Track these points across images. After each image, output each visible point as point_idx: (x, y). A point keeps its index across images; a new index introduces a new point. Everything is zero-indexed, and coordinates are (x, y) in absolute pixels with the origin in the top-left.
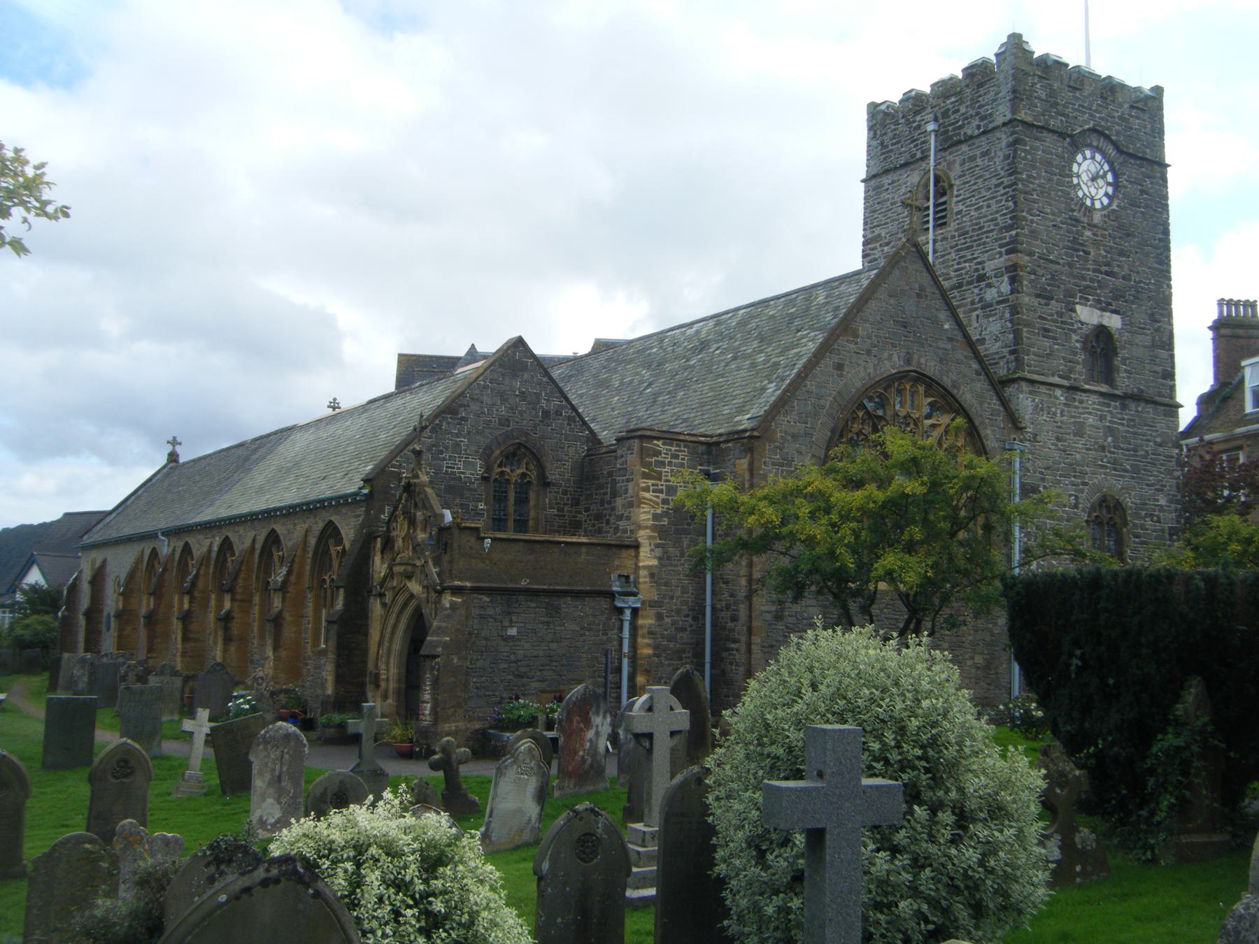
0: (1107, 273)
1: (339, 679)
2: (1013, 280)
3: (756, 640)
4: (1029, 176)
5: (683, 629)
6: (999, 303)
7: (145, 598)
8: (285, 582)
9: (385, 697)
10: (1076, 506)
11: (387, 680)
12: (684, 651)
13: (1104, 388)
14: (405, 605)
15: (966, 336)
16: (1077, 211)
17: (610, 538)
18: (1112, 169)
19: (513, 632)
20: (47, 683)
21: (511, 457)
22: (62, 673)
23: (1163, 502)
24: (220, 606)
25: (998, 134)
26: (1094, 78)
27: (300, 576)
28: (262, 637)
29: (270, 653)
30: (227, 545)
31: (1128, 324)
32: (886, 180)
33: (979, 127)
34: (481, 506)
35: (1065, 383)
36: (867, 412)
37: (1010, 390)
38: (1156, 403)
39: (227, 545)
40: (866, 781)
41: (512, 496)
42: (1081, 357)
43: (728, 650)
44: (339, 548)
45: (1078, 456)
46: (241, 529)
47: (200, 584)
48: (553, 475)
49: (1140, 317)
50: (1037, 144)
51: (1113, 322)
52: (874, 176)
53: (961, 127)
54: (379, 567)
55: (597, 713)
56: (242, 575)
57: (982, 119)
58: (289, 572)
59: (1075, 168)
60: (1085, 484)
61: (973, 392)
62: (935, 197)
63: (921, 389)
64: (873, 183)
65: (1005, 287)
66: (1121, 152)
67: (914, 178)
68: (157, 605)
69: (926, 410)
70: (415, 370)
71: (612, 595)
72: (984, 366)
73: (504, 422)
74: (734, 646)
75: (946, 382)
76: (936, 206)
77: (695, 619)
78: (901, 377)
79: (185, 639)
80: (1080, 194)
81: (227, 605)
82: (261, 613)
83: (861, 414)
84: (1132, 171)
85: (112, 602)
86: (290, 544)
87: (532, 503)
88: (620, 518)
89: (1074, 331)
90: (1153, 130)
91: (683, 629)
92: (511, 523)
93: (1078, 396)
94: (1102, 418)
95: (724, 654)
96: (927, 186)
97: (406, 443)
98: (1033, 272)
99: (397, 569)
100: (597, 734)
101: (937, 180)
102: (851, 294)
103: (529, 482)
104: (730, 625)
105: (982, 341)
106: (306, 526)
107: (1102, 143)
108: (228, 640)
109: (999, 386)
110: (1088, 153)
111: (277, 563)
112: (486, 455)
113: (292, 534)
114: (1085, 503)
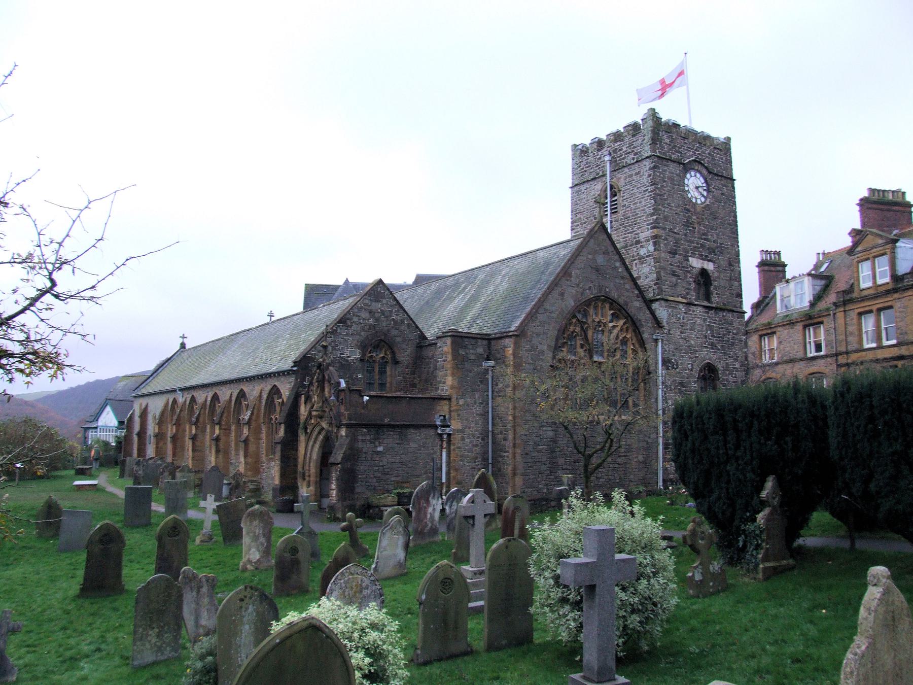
0: (705, 239)
1: (283, 475)
2: (655, 244)
3: (518, 451)
4: (662, 186)
5: (477, 445)
6: (648, 256)
7: (170, 426)
8: (250, 419)
9: (309, 486)
10: (692, 370)
11: (309, 476)
12: (477, 458)
13: (706, 303)
14: (319, 433)
15: (631, 275)
16: (688, 206)
17: (434, 394)
18: (706, 181)
19: (380, 449)
20: (118, 473)
21: (377, 347)
22: (127, 468)
23: (737, 366)
24: (213, 432)
25: (644, 163)
26: (695, 133)
27: (258, 416)
28: (237, 450)
29: (242, 459)
30: (215, 398)
31: (718, 267)
32: (583, 187)
33: (633, 159)
34: (360, 376)
35: (684, 301)
36: (578, 320)
37: (655, 306)
38: (733, 311)
39: (215, 398)
40: (618, 556)
41: (377, 369)
42: (693, 286)
43: (502, 456)
44: (280, 400)
45: (693, 342)
46: (223, 388)
47: (201, 420)
48: (400, 358)
49: (723, 262)
50: (666, 168)
51: (710, 266)
52: (576, 185)
53: (624, 158)
54: (303, 410)
55: (433, 497)
56: (225, 415)
57: (635, 154)
58: (252, 414)
59: (686, 181)
60: (696, 357)
61: (636, 305)
62: (611, 198)
63: (607, 306)
64: (576, 188)
65: (651, 248)
66: (710, 173)
67: (598, 186)
68: (177, 430)
69: (609, 318)
70: (316, 294)
71: (436, 427)
72: (641, 294)
73: (372, 327)
74: (505, 454)
75: (621, 301)
76: (611, 202)
77: (483, 439)
78: (597, 298)
79: (194, 450)
80: (689, 196)
81: (217, 432)
82: (236, 436)
83: (574, 320)
84: (716, 183)
85: (152, 428)
86: (252, 398)
87: (388, 373)
88: (440, 382)
89: (689, 272)
90: (726, 160)
91: (477, 445)
92: (376, 386)
93: (692, 308)
94: (705, 320)
95: (500, 459)
96: (606, 190)
97: (318, 341)
98: (666, 239)
99: (314, 413)
100: (434, 510)
101: (612, 187)
102: (564, 252)
103: (387, 362)
104: (503, 442)
105: (639, 278)
106: (260, 388)
107: (700, 168)
108: (218, 451)
109: (648, 303)
110: (693, 173)
111: (244, 408)
112: (363, 347)
113: (253, 391)
114: (697, 368)
